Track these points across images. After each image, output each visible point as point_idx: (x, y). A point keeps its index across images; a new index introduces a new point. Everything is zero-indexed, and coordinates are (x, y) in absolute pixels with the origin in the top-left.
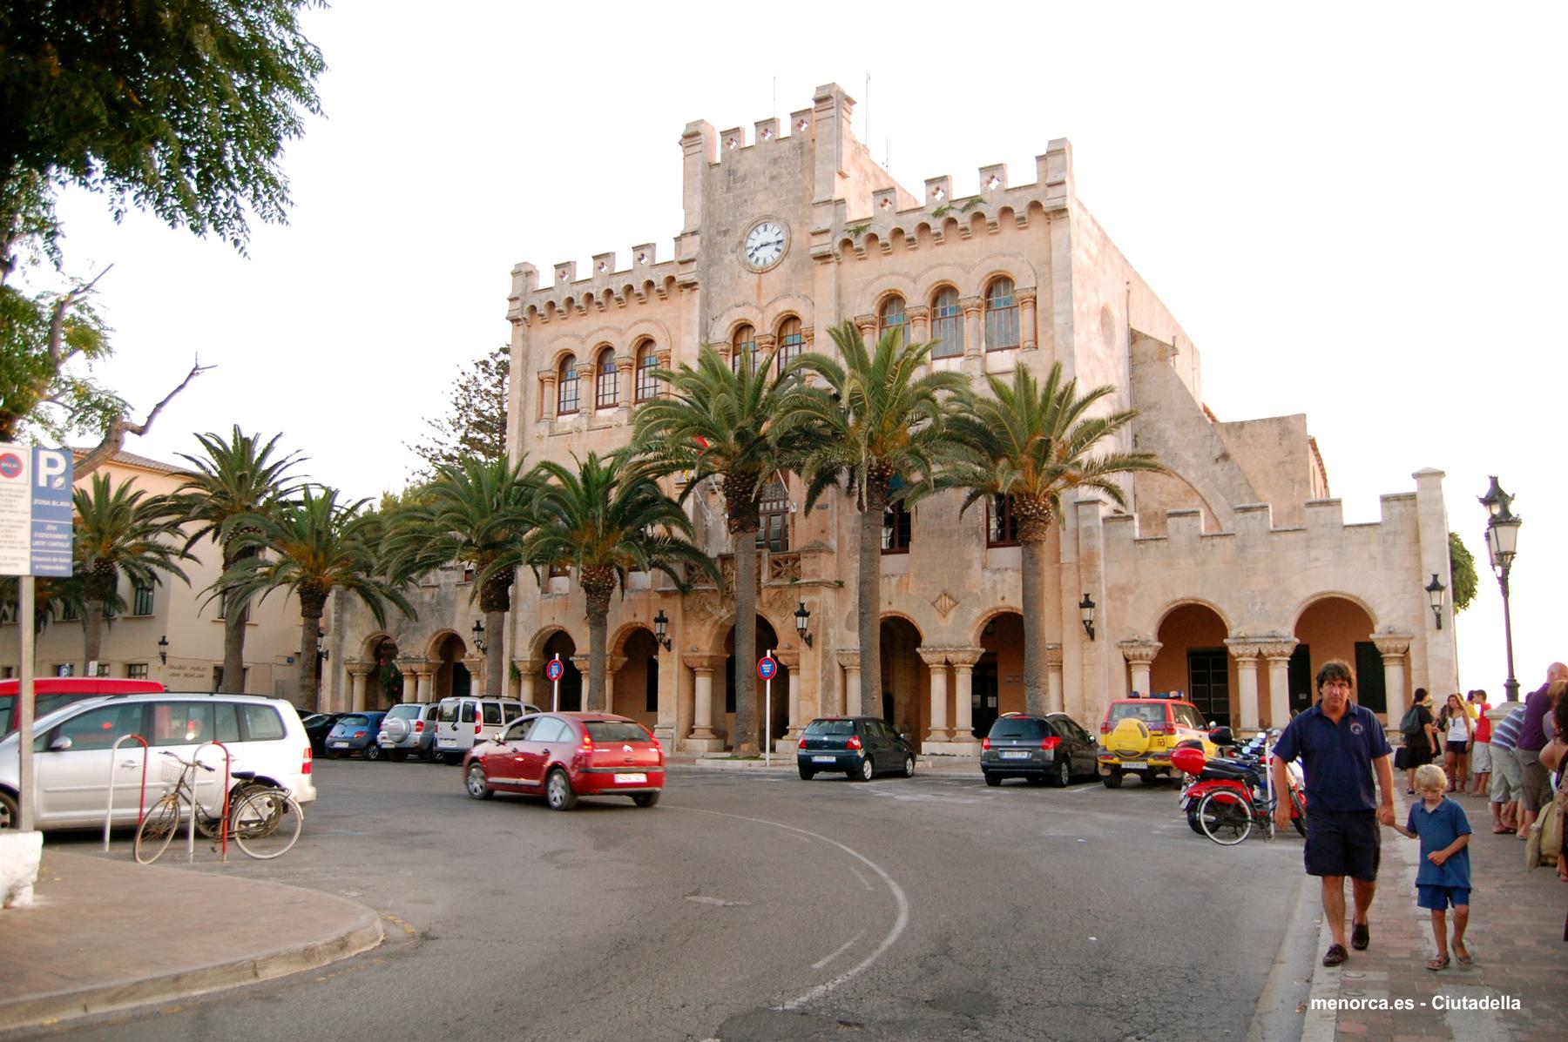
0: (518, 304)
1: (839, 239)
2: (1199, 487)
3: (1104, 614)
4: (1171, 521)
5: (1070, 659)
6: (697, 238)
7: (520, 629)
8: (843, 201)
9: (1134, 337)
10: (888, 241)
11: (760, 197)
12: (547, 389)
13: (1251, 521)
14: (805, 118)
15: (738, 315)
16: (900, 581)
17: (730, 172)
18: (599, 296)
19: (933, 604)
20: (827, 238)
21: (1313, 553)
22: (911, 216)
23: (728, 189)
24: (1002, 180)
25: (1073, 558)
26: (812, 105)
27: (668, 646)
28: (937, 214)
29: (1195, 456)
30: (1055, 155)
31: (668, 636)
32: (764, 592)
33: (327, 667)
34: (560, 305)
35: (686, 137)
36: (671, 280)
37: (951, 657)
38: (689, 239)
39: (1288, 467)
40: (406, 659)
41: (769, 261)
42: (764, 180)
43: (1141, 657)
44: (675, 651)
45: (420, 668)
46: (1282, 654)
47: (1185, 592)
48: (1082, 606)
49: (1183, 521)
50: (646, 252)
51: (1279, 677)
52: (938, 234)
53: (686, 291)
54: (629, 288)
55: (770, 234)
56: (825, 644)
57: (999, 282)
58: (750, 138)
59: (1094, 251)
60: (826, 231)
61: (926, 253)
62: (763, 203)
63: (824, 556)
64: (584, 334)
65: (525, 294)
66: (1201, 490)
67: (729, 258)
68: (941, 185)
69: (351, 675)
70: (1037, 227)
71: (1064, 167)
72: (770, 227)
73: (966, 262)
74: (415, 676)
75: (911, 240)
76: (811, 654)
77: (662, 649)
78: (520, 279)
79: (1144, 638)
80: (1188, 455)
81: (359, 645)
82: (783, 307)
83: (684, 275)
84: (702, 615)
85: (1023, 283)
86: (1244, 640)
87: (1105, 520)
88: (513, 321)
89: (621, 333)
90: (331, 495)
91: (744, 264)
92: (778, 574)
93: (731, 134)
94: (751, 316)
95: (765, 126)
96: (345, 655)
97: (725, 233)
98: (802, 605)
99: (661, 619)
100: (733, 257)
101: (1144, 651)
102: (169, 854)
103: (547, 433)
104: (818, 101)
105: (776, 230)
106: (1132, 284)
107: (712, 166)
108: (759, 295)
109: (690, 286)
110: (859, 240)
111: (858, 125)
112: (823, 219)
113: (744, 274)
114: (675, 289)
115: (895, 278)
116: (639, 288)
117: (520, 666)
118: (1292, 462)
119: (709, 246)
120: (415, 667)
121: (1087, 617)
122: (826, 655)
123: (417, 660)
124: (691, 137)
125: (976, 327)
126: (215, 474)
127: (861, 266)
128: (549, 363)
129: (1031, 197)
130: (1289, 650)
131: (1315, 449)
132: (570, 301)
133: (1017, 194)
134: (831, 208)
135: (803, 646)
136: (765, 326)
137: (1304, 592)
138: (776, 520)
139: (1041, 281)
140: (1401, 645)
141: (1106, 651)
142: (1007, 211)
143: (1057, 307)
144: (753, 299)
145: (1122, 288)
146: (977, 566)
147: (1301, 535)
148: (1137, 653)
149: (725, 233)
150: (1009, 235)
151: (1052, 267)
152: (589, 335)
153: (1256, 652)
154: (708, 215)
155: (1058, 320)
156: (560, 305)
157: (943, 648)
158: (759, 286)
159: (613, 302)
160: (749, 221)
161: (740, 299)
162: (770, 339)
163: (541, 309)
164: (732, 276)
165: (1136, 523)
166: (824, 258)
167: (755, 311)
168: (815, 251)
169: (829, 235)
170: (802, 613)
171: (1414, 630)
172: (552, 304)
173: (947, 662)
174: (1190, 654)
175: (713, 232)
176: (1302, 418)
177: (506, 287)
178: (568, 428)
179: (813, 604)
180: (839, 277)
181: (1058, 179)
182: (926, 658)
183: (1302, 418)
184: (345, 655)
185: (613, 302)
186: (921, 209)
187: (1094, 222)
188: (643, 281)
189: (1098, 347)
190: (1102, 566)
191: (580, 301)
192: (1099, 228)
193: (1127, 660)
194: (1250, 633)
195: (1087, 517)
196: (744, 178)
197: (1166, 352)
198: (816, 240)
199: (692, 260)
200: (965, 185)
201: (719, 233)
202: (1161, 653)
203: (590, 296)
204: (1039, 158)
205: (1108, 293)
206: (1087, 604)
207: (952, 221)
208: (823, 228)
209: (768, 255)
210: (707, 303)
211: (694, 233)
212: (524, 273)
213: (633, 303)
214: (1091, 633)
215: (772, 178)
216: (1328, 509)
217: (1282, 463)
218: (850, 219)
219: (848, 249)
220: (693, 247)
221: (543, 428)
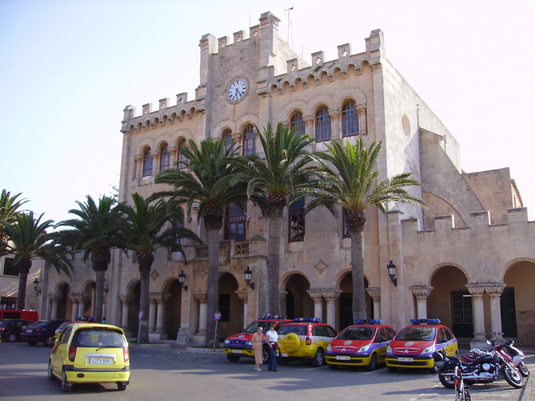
0: (126, 124)
1: (270, 85)
2: (455, 206)
3: (402, 271)
4: (436, 221)
5: (385, 295)
6: (205, 89)
7: (123, 280)
8: (272, 67)
9: (421, 132)
10: (294, 85)
11: (235, 68)
12: (138, 164)
13: (478, 221)
14: (256, 30)
15: (224, 125)
16: (299, 256)
17: (222, 57)
18: (161, 119)
19: (315, 267)
20: (265, 84)
21: (512, 237)
22: (305, 72)
23: (221, 65)
24: (349, 52)
25: (386, 242)
26: (259, 23)
27: (186, 288)
28: (316, 70)
29: (453, 190)
31: (186, 284)
32: (232, 262)
34: (144, 124)
35: (201, 41)
36: (193, 109)
37: (324, 294)
38: (202, 89)
39: (501, 195)
40: (74, 294)
42: (237, 60)
43: (422, 294)
44: (189, 291)
45: (80, 298)
46: (497, 292)
47: (443, 260)
48: (389, 267)
49: (443, 221)
50: (183, 97)
51: (496, 305)
52: (318, 80)
53: (200, 114)
55: (240, 86)
56: (260, 288)
57: (348, 105)
58: (231, 41)
59: (398, 87)
60: (264, 81)
61: (311, 90)
62: (237, 71)
63: (259, 243)
64: (154, 137)
65: (129, 120)
66: (456, 208)
68: (319, 56)
70: (365, 75)
72: (239, 82)
73: (332, 93)
75: (305, 83)
77: (183, 291)
79: (423, 284)
81: (54, 287)
82: (245, 120)
83: (199, 107)
84: (203, 273)
85: (360, 102)
86: (315, 290)
87: (403, 222)
88: (123, 132)
89: (171, 136)
90: (32, 213)
91: (228, 100)
92: (239, 252)
93: (223, 40)
94: (231, 125)
95: (238, 34)
96: (49, 292)
97: (219, 86)
98: (248, 268)
99: (182, 275)
100: (222, 97)
103: (137, 185)
104: (261, 20)
105: (243, 83)
106: (420, 105)
110: (281, 85)
111: (280, 32)
112: (263, 75)
114: (195, 114)
116: (179, 114)
117: (122, 298)
118: (503, 192)
119: (211, 92)
120: (77, 298)
121: (391, 273)
122: (261, 294)
123: (78, 294)
124: (204, 41)
125: (338, 125)
127: (281, 98)
130: (500, 290)
131: (515, 186)
132: (148, 122)
133: (356, 58)
134: (267, 70)
135: (250, 289)
136: (236, 129)
138: (241, 226)
139: (369, 101)
141: (403, 291)
142: (351, 66)
143: (377, 113)
145: (415, 108)
146: (337, 247)
147: (506, 227)
148: (420, 292)
149: (219, 86)
150: (352, 78)
151: (375, 93)
152: (157, 137)
153: (482, 291)
154: (211, 77)
155: (377, 119)
156: (144, 124)
157: (321, 290)
158: (234, 111)
159: (168, 122)
160: (230, 80)
161: (225, 117)
162: (239, 136)
163: (136, 127)
164: (222, 107)
165: (419, 223)
166: (263, 94)
167: (232, 123)
168: (258, 91)
169: (266, 83)
170: (248, 272)
172: (140, 124)
173: (322, 297)
174: (452, 293)
175: (214, 86)
176: (507, 170)
177: (121, 116)
178: (147, 183)
179: (254, 267)
180: (270, 104)
181: (376, 49)
182: (312, 295)
183: (507, 170)
184: (49, 292)
185: (168, 122)
186: (310, 68)
187: (397, 72)
188: (180, 110)
189: (401, 135)
190: (400, 246)
191: (152, 122)
192: (400, 76)
193: (414, 296)
194: (480, 281)
195: (392, 220)
197: (437, 138)
198: (260, 86)
199: (202, 99)
200: (331, 55)
201: (216, 86)
202: (433, 292)
203: (157, 119)
204: (367, 40)
205: (408, 108)
206: (391, 265)
207: (325, 73)
208: (263, 80)
210: (209, 120)
211: (204, 87)
212: (128, 111)
213: (177, 121)
214: (395, 282)
215: (241, 59)
216: (520, 213)
217: (497, 193)
218: (276, 75)
219: (275, 90)
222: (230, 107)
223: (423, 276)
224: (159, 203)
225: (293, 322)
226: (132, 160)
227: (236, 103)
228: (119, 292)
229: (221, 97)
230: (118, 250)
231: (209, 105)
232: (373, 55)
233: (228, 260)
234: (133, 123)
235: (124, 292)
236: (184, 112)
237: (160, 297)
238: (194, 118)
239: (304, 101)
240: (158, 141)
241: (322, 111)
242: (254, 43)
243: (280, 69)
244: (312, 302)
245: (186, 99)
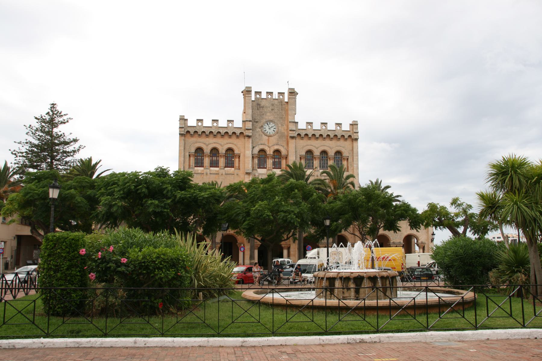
0: (183, 129)
1: (297, 133)
11: (268, 114)
12: (192, 158)
15: (262, 147)
24: (217, 124)
30: (354, 125)
41: (271, 133)
42: (270, 109)
58: (264, 96)
67: (258, 130)
71: (357, 128)
76: (294, 244)
78: (183, 122)
82: (276, 147)
83: (249, 133)
85: (345, 154)
91: (263, 133)
97: (257, 122)
100: (260, 130)
102: (402, 313)
107: (253, 101)
108: (268, 143)
109: (249, 137)
113: (263, 135)
124: (247, 92)
127: (301, 141)
128: (193, 150)
140: (423, 245)
144: (266, 143)
151: (353, 152)
158: (268, 140)
164: (259, 135)
166: (292, 138)
171: (426, 242)
196: (263, 107)
198: (291, 132)
204: (351, 124)
212: (183, 119)
213: (226, 137)
215: (272, 110)
220: (249, 125)
226: (187, 154)
232: (355, 134)
238: (240, 138)
240: (211, 147)
241: (324, 153)
243: (302, 125)
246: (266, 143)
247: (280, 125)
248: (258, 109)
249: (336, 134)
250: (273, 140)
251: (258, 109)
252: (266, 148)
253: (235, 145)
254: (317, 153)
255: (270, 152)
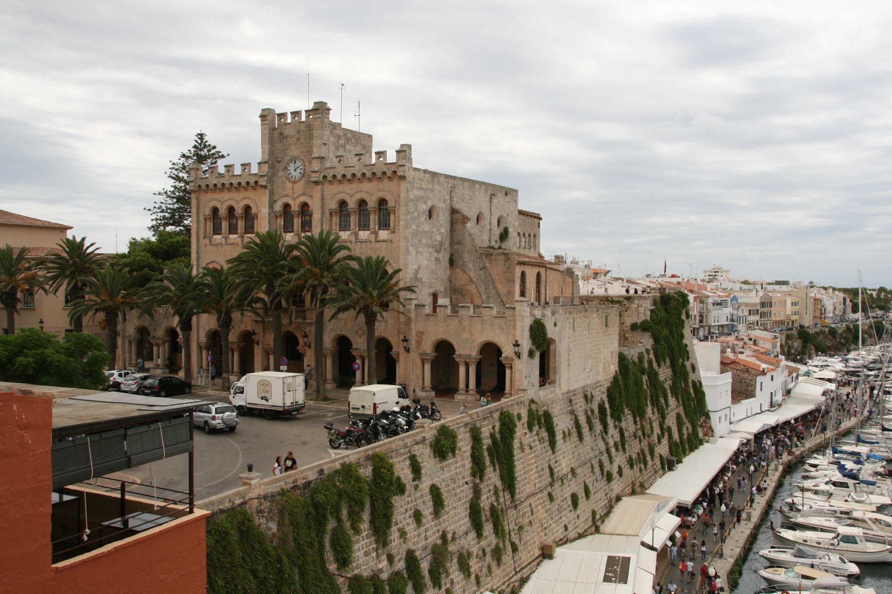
1: (322, 175)
6: (267, 165)
7: (201, 329)
11: (293, 147)
15: (285, 200)
17: (281, 134)
20: (317, 175)
24: (385, 159)
27: (258, 343)
33: (119, 341)
34: (211, 187)
40: (154, 338)
47: (441, 336)
54: (239, 184)
62: (294, 151)
67: (281, 173)
69: (130, 343)
70: (395, 182)
73: (371, 192)
74: (158, 345)
80: (471, 266)
82: (302, 199)
83: (262, 182)
85: (391, 204)
86: (460, 355)
87: (416, 306)
91: (287, 178)
95: (296, 114)
97: (279, 162)
101: (429, 357)
109: (265, 187)
112: (316, 166)
115: (344, 195)
119: (272, 167)
123: (158, 339)
125: (374, 219)
126: (65, 255)
127: (331, 187)
129: (393, 168)
132: (215, 185)
137: (481, 338)
141: (414, 356)
142: (384, 173)
144: (290, 194)
154: (272, 152)
158: (293, 188)
161: (286, 193)
163: (203, 187)
166: (316, 183)
180: (322, 190)
182: (354, 353)
184: (127, 334)
198: (313, 175)
204: (397, 152)
206: (405, 340)
209: (296, 174)
210: (272, 193)
215: (298, 140)
221: (207, 241)
222: (289, 185)
223: (428, 347)
224: (130, 352)
225: (188, 347)
226: (202, 218)
227: (294, 182)
228: (198, 339)
229: (281, 173)
230: (55, 411)
231: (271, 180)
233: (291, 322)
234: (200, 183)
235: (203, 339)
236: (248, 183)
237: (236, 346)
239: (348, 194)
240: (226, 204)
242: (309, 126)
244: (456, 366)
245: (250, 170)
246: (290, 194)
247: (307, 164)
248: (281, 142)
249: (374, 170)
250: (299, 187)
251: (281, 142)
252: (291, 202)
253: (344, 192)
254: (352, 204)
255: (295, 207)
